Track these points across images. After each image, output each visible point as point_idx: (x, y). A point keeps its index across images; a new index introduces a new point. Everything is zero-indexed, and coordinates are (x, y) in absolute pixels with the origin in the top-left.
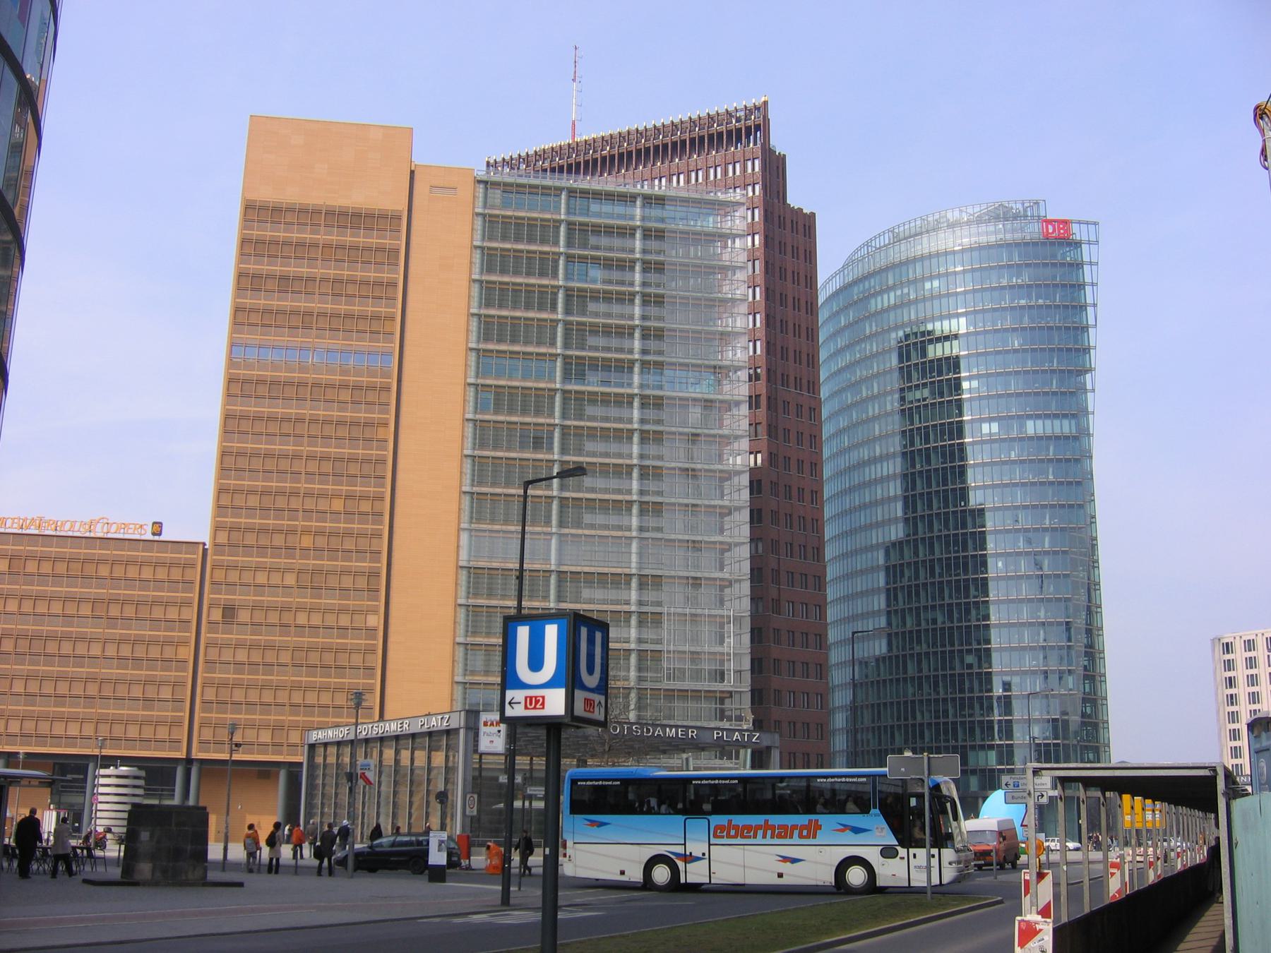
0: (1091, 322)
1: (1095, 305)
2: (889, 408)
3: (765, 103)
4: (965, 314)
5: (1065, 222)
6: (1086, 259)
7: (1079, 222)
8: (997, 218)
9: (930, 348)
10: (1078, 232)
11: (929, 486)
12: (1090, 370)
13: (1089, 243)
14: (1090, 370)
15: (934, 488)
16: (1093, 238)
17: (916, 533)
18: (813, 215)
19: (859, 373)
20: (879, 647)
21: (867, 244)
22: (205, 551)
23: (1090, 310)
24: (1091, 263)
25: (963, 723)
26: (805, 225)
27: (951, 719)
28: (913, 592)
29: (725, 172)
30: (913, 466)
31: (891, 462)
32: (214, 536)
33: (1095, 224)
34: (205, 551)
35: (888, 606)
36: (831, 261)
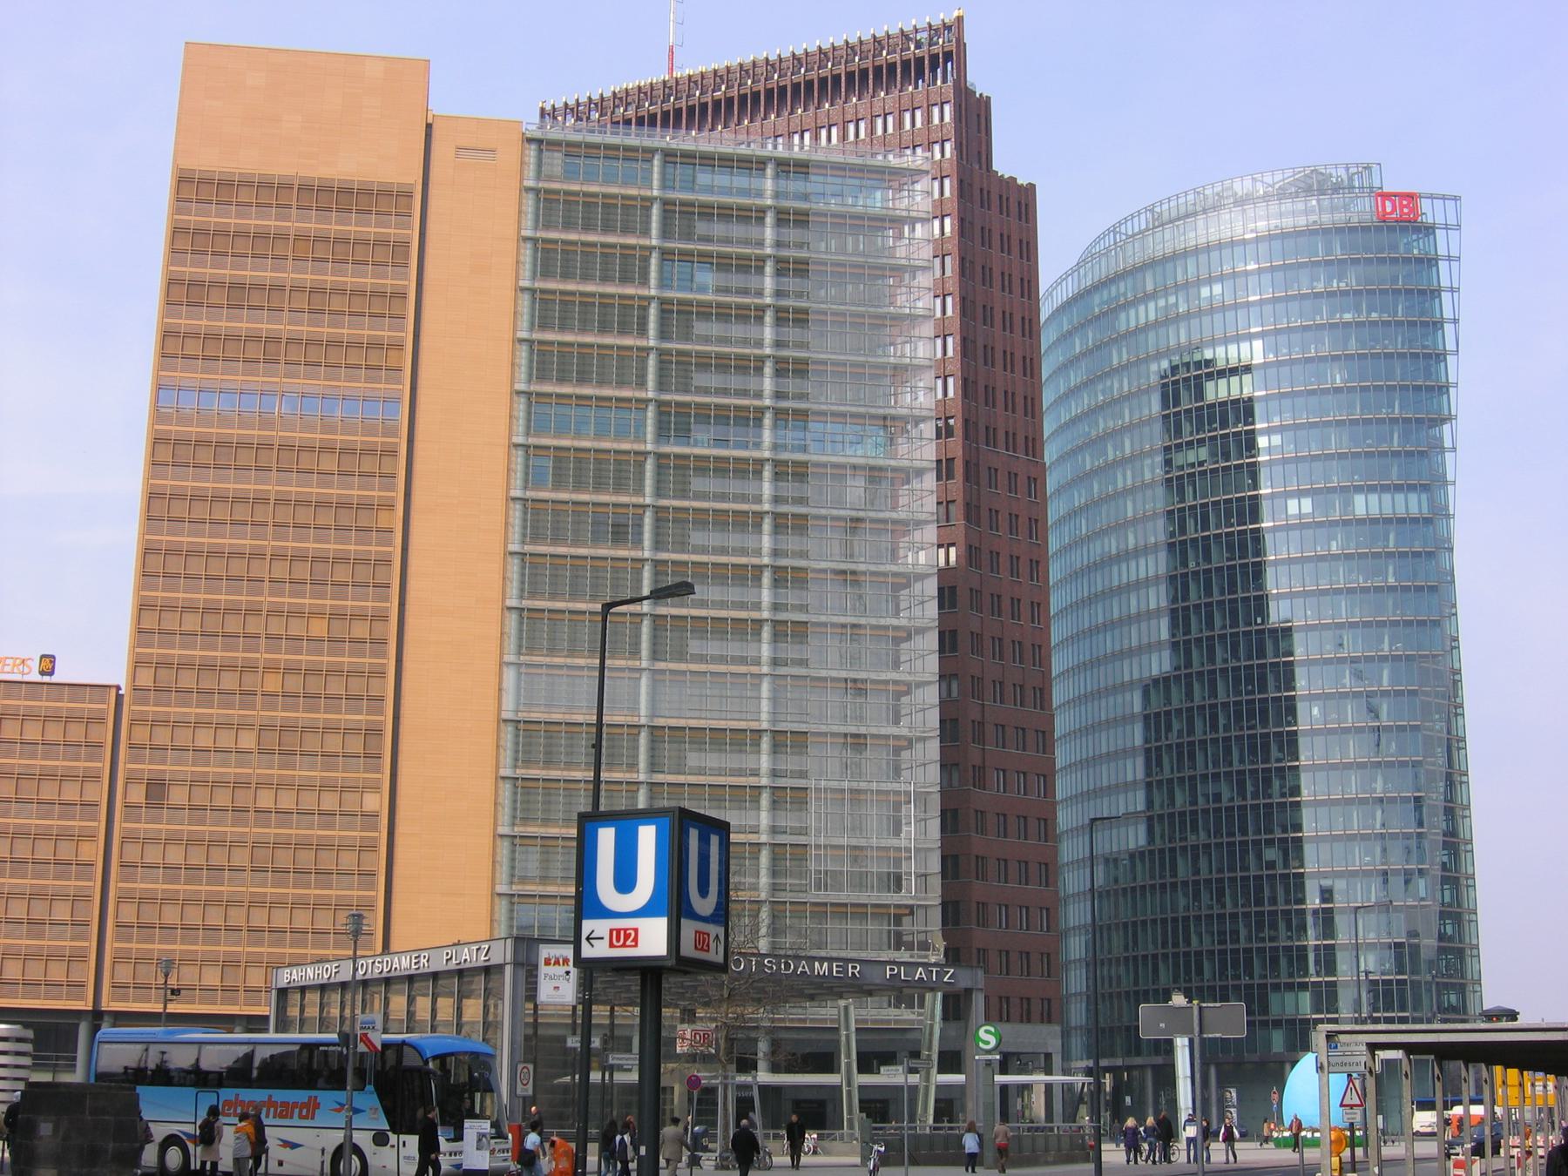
0: (1450, 346)
1: (1455, 321)
2: (1148, 476)
3: (960, 19)
4: (1262, 335)
5: (1411, 197)
6: (1442, 251)
7: (1432, 197)
8: (1309, 191)
9: (1209, 386)
10: (1430, 212)
11: (1209, 593)
12: (1449, 418)
13: (1447, 227)
14: (1449, 418)
15: (1216, 597)
16: (1452, 220)
17: (1189, 664)
18: (989, 98)
19: (1103, 424)
20: (1135, 837)
21: (1113, 230)
22: (119, 698)
23: (1448, 328)
24: (1449, 258)
25: (1261, 951)
26: (1018, 204)
27: (1243, 944)
28: (1185, 753)
29: (900, 124)
30: (1185, 564)
31: (1151, 559)
32: (133, 676)
33: (1456, 199)
34: (119, 698)
35: (1148, 773)
36: (1060, 256)
